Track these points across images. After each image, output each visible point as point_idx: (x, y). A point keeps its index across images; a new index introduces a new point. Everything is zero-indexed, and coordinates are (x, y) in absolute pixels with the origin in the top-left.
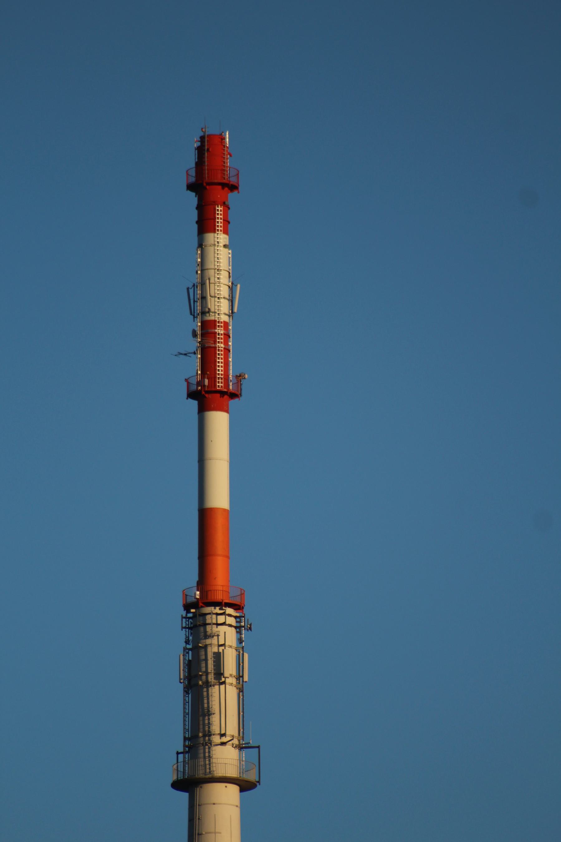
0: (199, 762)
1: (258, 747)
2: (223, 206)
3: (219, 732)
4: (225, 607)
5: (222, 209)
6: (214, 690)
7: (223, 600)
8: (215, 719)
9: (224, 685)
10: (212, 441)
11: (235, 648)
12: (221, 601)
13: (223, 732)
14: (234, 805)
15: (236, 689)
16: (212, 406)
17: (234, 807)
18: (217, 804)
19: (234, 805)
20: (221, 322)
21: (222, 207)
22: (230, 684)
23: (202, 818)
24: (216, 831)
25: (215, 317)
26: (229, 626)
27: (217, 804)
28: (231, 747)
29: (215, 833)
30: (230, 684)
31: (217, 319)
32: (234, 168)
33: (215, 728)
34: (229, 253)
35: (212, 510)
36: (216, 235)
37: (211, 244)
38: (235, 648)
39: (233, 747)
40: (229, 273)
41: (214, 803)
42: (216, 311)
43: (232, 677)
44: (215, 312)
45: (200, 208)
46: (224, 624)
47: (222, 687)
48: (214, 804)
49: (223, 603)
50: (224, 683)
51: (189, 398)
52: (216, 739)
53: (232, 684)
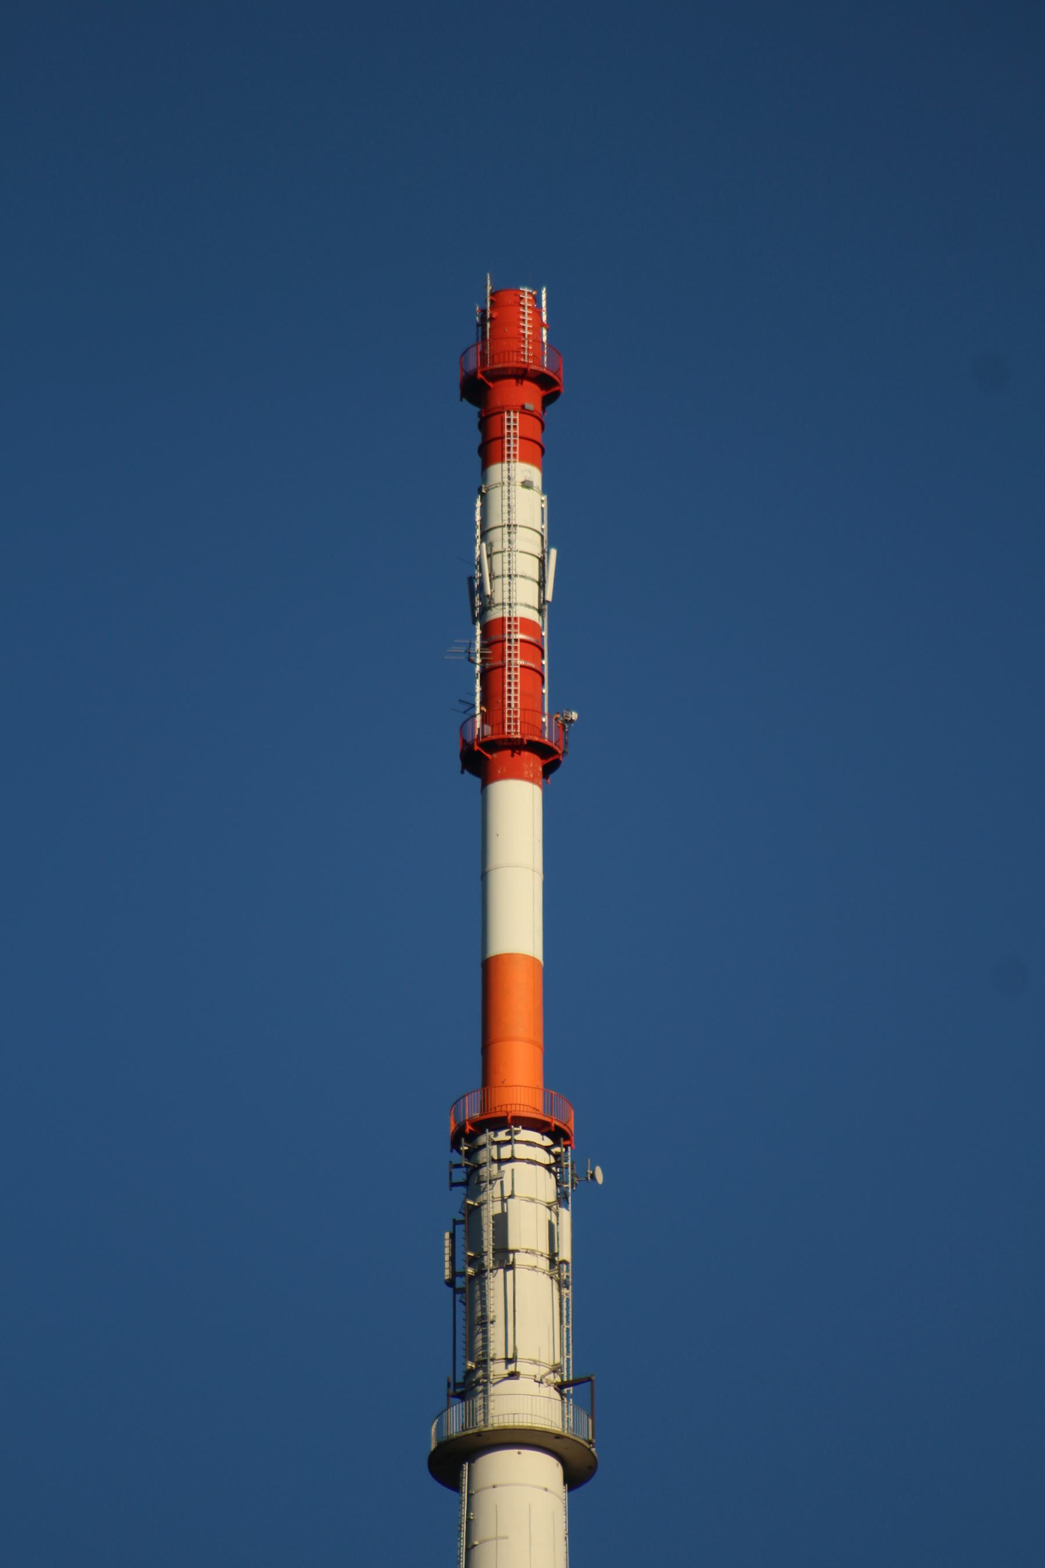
0: (476, 1416)
1: (589, 1379)
2: (520, 413)
3: (504, 1357)
4: (516, 1126)
5: (517, 417)
6: (495, 1281)
7: (508, 1114)
8: (496, 1332)
9: (512, 1271)
10: (498, 835)
11: (547, 1205)
12: (506, 1115)
13: (510, 1356)
14: (540, 1488)
15: (550, 1280)
16: (499, 772)
17: (541, 1490)
18: (501, 1485)
19: (540, 1488)
20: (516, 619)
21: (518, 413)
22: (530, 1268)
23: (475, 1517)
24: (498, 1535)
25: (503, 613)
26: (528, 1163)
27: (501, 1485)
28: (533, 1380)
29: (496, 1539)
30: (532, 1267)
31: (506, 615)
32: (554, 349)
33: (497, 1348)
34: (542, 501)
35: (497, 957)
36: (505, 465)
37: (497, 484)
38: (547, 1205)
39: (535, 1381)
40: (542, 537)
41: (493, 1484)
42: (506, 601)
43: (537, 1255)
44: (503, 604)
45: (484, 424)
46: (512, 1159)
47: (510, 1273)
48: (494, 1487)
49: (509, 1118)
50: (512, 1267)
51: (466, 772)
52: (498, 1369)
53: (536, 1267)
